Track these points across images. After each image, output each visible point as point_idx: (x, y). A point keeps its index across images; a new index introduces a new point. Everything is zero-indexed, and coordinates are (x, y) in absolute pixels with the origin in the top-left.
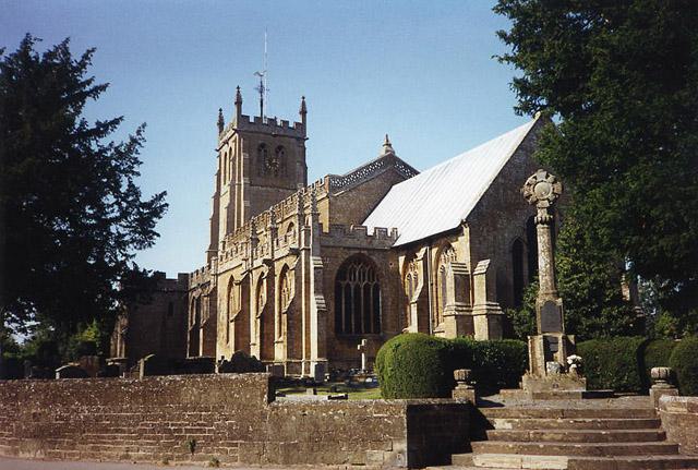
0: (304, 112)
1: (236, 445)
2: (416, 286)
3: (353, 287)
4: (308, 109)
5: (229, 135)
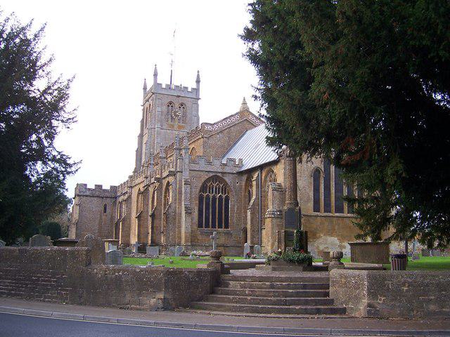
0: (198, 82)
5: (149, 96)
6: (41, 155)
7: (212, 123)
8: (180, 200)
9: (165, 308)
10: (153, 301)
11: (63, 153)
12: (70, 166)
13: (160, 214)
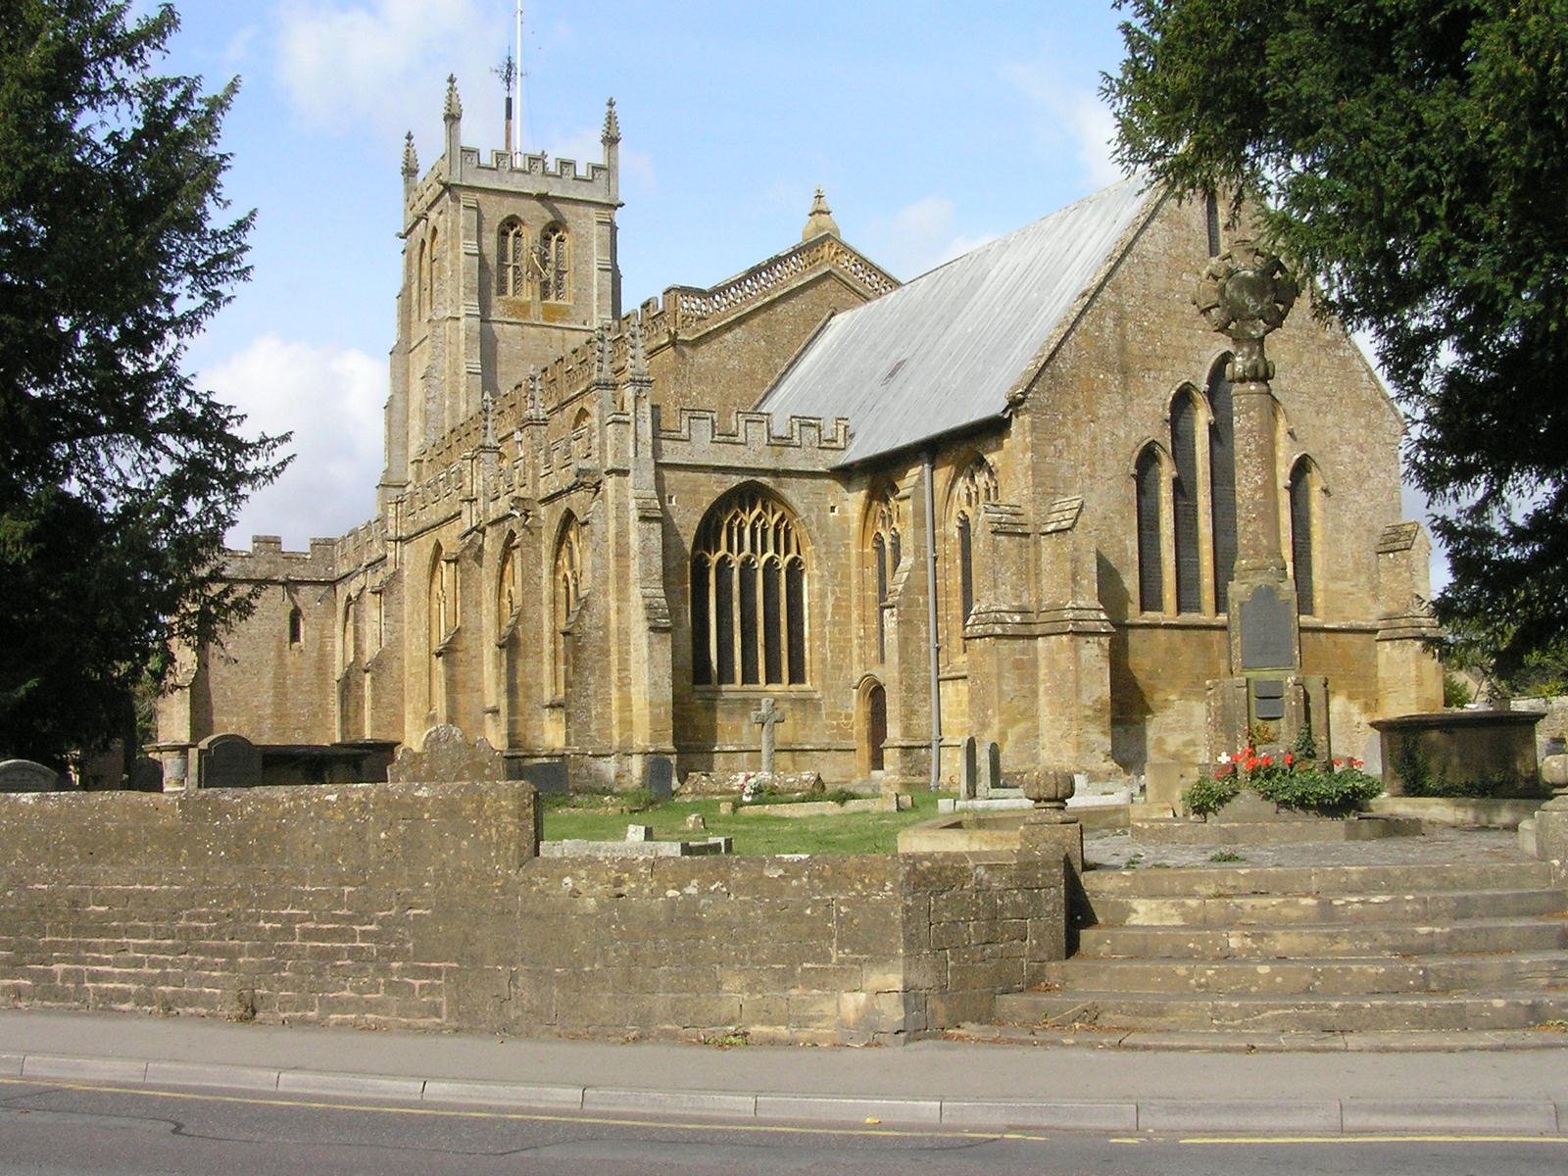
0: (611, 141)
1: (438, 973)
2: (896, 563)
3: (736, 566)
4: (624, 130)
6: (125, 407)
7: (707, 287)
8: (622, 577)
9: (914, 1031)
10: (852, 1003)
11: (213, 398)
12: (239, 446)
13: (539, 640)
